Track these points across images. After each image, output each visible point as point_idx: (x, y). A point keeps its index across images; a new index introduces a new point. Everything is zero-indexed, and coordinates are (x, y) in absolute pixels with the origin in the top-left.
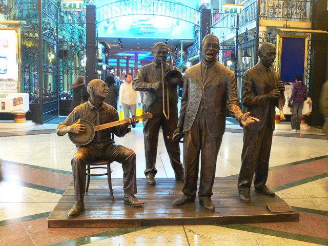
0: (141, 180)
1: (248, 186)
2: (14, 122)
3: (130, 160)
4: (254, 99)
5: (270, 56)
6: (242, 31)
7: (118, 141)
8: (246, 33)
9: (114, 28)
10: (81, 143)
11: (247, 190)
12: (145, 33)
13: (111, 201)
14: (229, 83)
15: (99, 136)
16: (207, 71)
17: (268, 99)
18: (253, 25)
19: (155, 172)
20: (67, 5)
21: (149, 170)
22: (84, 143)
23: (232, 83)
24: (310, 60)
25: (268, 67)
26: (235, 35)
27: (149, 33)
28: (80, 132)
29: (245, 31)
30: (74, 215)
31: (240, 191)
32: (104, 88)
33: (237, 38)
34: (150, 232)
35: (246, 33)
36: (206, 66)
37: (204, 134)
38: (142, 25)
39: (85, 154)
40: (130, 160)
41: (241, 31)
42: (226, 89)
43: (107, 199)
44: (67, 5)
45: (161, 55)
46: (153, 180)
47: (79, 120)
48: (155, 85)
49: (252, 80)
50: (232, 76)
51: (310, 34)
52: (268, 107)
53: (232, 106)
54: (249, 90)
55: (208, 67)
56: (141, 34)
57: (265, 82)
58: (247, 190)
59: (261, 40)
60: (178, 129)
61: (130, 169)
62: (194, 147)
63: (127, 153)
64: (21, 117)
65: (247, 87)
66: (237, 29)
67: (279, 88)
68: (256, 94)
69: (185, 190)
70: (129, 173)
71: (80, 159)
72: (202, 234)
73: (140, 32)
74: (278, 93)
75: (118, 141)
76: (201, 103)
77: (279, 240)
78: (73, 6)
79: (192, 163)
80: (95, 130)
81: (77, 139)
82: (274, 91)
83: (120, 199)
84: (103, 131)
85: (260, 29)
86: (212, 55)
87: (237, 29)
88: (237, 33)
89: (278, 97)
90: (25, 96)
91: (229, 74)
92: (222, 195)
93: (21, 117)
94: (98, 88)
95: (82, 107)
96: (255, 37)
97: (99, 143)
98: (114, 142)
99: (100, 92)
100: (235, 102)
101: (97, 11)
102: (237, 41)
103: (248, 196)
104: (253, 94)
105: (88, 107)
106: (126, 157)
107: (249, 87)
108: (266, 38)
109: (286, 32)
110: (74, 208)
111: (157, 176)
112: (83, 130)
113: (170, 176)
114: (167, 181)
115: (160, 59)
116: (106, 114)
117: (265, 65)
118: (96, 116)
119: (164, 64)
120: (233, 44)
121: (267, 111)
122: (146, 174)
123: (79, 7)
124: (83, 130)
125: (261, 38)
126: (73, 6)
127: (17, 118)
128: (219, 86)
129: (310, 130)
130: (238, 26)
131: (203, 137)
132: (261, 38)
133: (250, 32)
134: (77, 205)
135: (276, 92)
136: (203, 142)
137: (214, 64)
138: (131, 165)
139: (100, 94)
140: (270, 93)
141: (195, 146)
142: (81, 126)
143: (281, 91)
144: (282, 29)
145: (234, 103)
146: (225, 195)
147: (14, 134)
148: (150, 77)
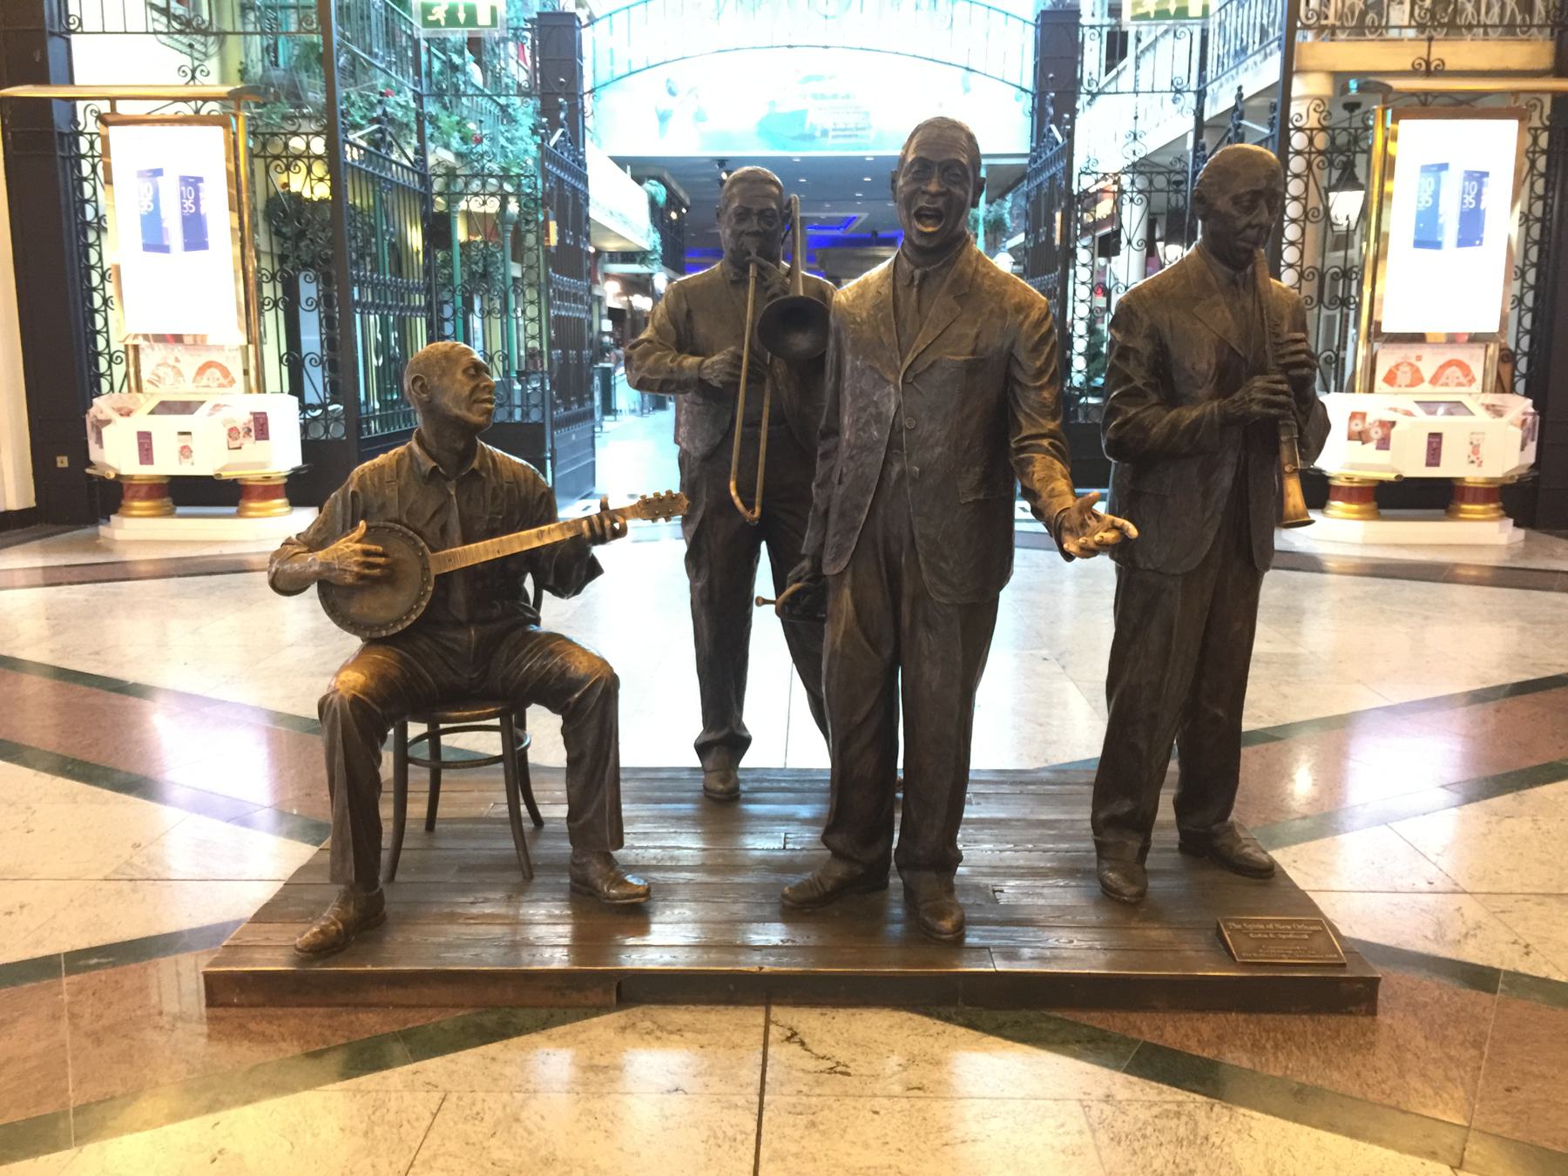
0: (685, 775)
1: (1143, 823)
2: (239, 515)
3: (593, 700)
4: (1160, 421)
5: (1251, 208)
6: (1220, 101)
7: (555, 613)
8: (1237, 112)
9: (699, 117)
10: (369, 627)
11: (1134, 844)
12: (825, 133)
13: (515, 877)
14: (1022, 356)
15: (459, 595)
16: (919, 302)
17: (1227, 421)
18: (1267, 72)
19: (741, 743)
20: (439, 14)
21: (711, 736)
22: (384, 626)
23: (1036, 349)
24: (1541, 220)
25: (1239, 266)
26: (1190, 123)
27: (846, 133)
28: (361, 577)
29: (1231, 102)
30: (321, 950)
31: (1100, 846)
32: (473, 384)
33: (1198, 135)
34: (610, 1034)
35: (1235, 108)
36: (917, 273)
37: (907, 587)
38: (815, 96)
39: (381, 678)
40: (593, 700)
41: (1215, 101)
42: (1009, 381)
43: (498, 866)
44: (439, 14)
45: (753, 225)
46: (724, 781)
47: (362, 523)
48: (714, 364)
49: (1155, 335)
50: (1035, 315)
51: (1547, 100)
52: (1231, 458)
53: (1030, 462)
54: (1139, 383)
55: (924, 277)
56: (810, 137)
57: (1222, 344)
58: (1134, 844)
59: (1298, 141)
60: (806, 564)
61: (590, 740)
62: (866, 645)
63: (580, 667)
64: (266, 491)
65: (1130, 368)
66: (1201, 95)
67: (1286, 368)
68: (1172, 400)
69: (837, 840)
70: (587, 760)
71: (355, 700)
72: (841, 1054)
73: (807, 130)
74: (1028, 415)
75: (555, 613)
76: (889, 448)
77: (1201, 1115)
78: (462, 17)
79: (858, 718)
80: (435, 570)
81: (355, 608)
82: (1259, 382)
83: (553, 867)
84: (475, 573)
85: (1299, 86)
86: (937, 216)
87: (1201, 95)
88: (1199, 112)
89: (1273, 411)
90: (285, 415)
91: (1022, 308)
92: (1010, 857)
93: (266, 491)
94: (446, 381)
95: (382, 467)
96: (1271, 125)
97: (459, 625)
98: (537, 621)
99: (457, 399)
100: (1045, 442)
101: (586, 35)
102: (1198, 147)
103: (1136, 867)
104: (1154, 398)
105: (411, 468)
106: (577, 683)
107: (1140, 364)
108: (1323, 129)
109: (1427, 93)
110: (328, 918)
111: (747, 761)
112: (377, 572)
113: (798, 761)
114: (794, 783)
115: (751, 245)
116: (495, 497)
117: (1224, 260)
118: (441, 509)
119: (761, 268)
120: (1178, 167)
121: (1226, 479)
122: (702, 748)
123: (488, 22)
124: (377, 572)
125: (1299, 129)
126: (462, 17)
127: (250, 499)
128: (973, 367)
129: (1527, 553)
130: (1202, 78)
131: (905, 608)
132: (1299, 129)
133: (1254, 103)
134: (344, 902)
135: (1265, 390)
136: (906, 621)
137: (950, 264)
138: (594, 723)
139: (456, 411)
140: (1237, 396)
141: (871, 644)
142: (366, 553)
143: (1292, 381)
144: (1398, 84)
145: (1040, 449)
146: (1021, 859)
147: (241, 563)
148: (702, 328)
